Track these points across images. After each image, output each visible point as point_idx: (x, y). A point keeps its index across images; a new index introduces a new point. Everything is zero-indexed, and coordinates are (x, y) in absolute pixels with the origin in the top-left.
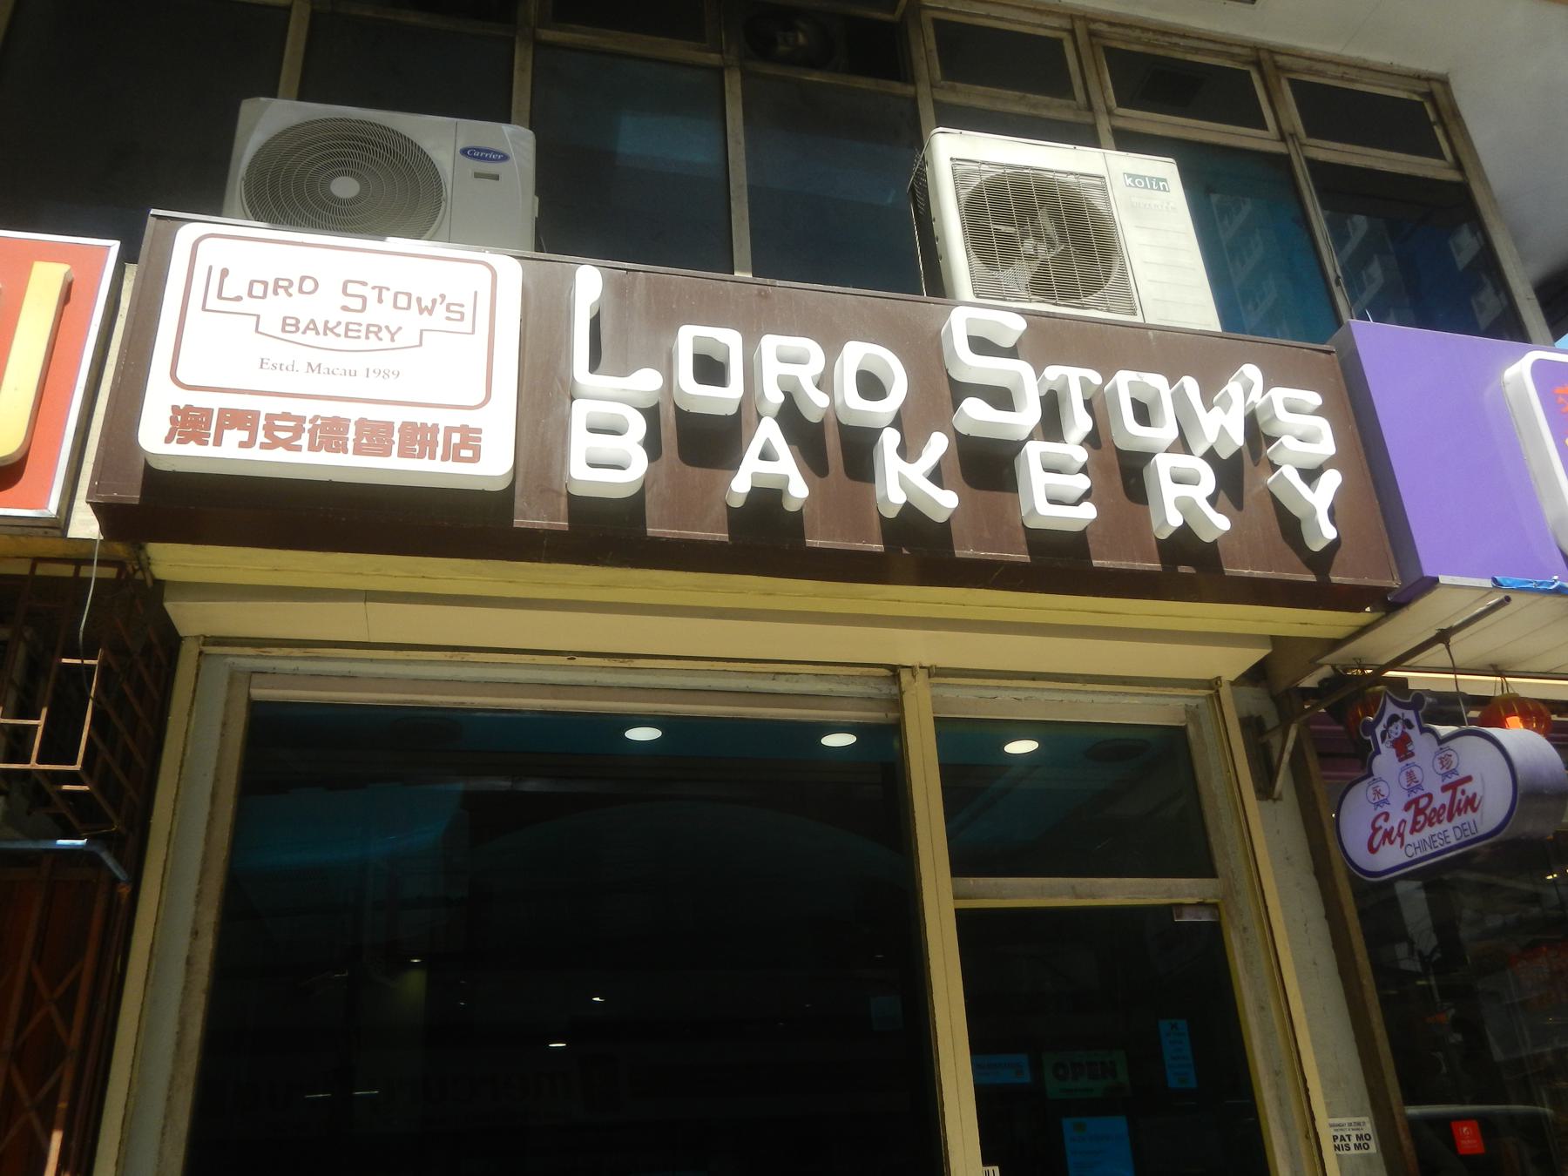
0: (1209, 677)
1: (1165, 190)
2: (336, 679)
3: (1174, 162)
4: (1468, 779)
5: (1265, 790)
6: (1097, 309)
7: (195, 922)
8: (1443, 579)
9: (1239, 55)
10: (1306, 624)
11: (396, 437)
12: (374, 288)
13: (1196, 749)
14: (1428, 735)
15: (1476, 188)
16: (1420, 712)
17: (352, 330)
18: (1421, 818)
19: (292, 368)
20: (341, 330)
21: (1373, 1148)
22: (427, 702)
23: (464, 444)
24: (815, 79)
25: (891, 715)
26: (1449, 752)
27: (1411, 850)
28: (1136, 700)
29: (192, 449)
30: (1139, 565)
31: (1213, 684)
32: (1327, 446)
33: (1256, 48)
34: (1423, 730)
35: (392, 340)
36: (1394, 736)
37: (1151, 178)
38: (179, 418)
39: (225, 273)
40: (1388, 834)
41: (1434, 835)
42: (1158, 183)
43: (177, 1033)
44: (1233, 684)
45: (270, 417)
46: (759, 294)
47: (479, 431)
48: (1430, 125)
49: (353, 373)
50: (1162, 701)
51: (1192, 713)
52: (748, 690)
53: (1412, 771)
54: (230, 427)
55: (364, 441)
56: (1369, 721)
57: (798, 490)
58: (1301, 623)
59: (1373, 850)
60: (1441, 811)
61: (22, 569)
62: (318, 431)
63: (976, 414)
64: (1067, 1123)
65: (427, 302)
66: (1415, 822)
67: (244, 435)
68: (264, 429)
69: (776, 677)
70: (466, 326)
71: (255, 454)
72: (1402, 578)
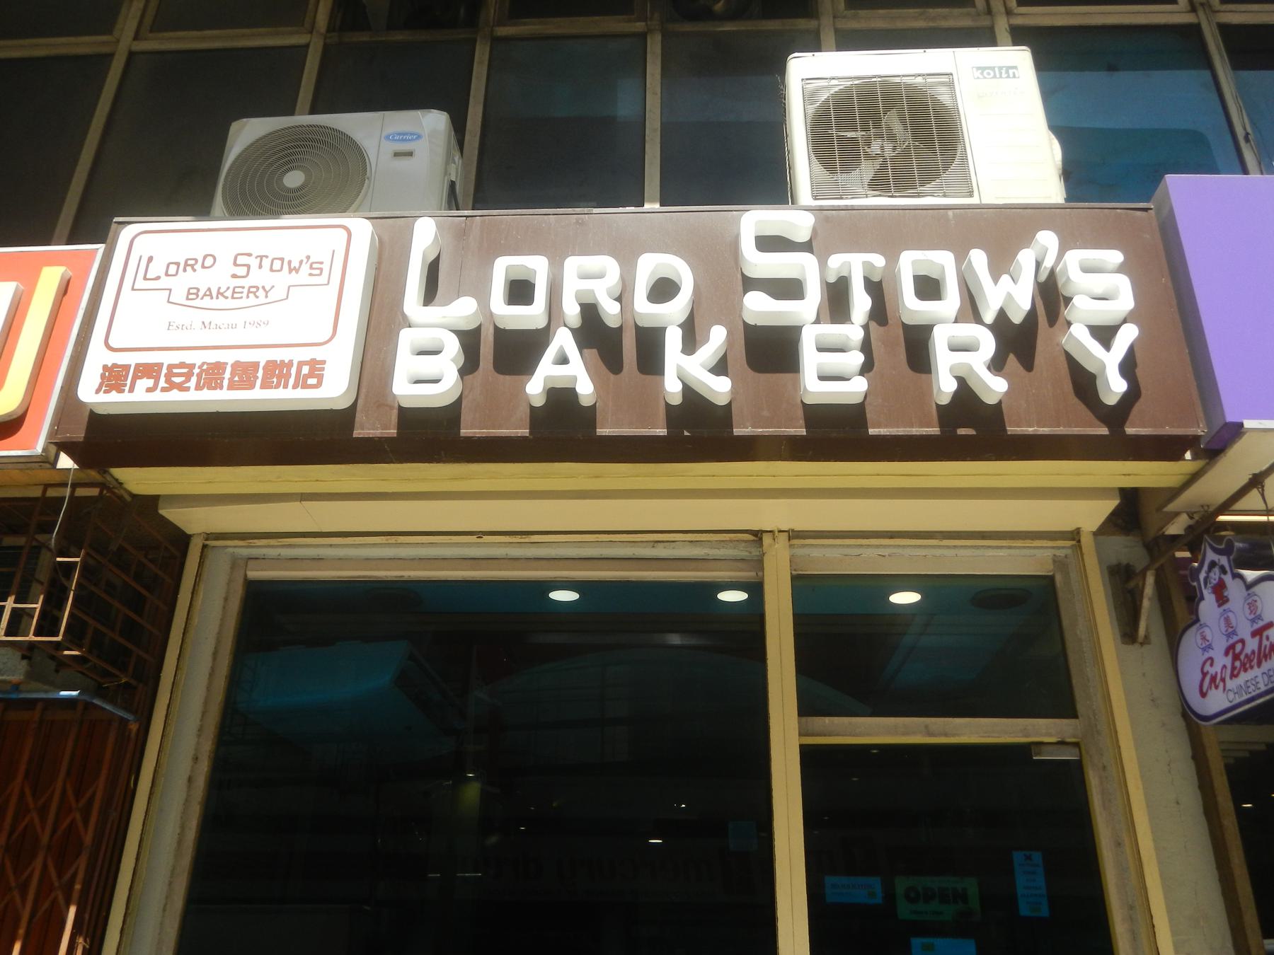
0: (1069, 529)
1: (1014, 77)
2: (308, 561)
3: (1029, 50)
5: (1129, 633)
6: (933, 196)
7: (196, 750)
8: (1248, 424)
10: (1129, 475)
11: (260, 374)
12: (256, 258)
14: (1238, 580)
16: (1231, 557)
17: (237, 293)
18: (1238, 664)
20: (229, 294)
22: (375, 577)
23: (311, 375)
25: (753, 574)
26: (1255, 598)
27: (1231, 696)
28: (1001, 553)
29: (114, 397)
30: (792, 431)
31: (1075, 535)
32: (1125, 301)
35: (266, 297)
37: (1000, 68)
38: (107, 374)
39: (150, 259)
40: (1213, 679)
41: (1248, 681)
42: (1009, 71)
43: (179, 834)
44: (1096, 534)
45: (170, 367)
46: (577, 222)
47: (324, 362)
49: (234, 326)
51: (1059, 563)
52: (603, 557)
53: (1228, 617)
54: (140, 378)
55: (236, 379)
56: (1194, 567)
57: (585, 388)
58: (1124, 475)
59: (1203, 695)
60: (1252, 656)
61: (36, 493)
62: (204, 374)
63: (759, 307)
64: (916, 942)
66: (1233, 668)
67: (150, 383)
68: (165, 376)
69: (656, 544)
70: (323, 279)
71: (158, 396)
72: (1209, 423)
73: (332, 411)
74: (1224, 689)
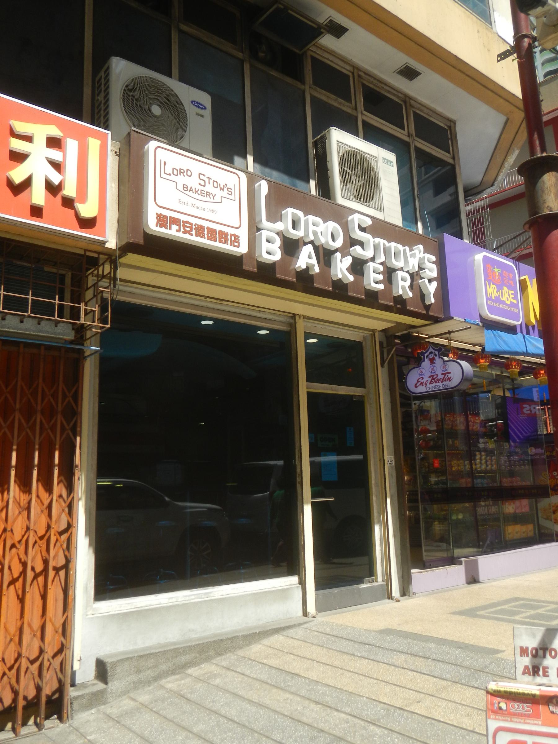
4: (450, 373)
5: (382, 366)
8: (454, 318)
9: (400, 97)
12: (207, 178)
13: (364, 349)
15: (457, 167)
18: (433, 381)
19: (187, 204)
20: (199, 192)
21: (393, 464)
24: (273, 74)
28: (352, 332)
31: (373, 331)
32: (434, 274)
33: (406, 95)
34: (439, 358)
36: (430, 357)
42: (390, 163)
45: (184, 222)
48: (448, 139)
50: (358, 333)
51: (365, 338)
59: (416, 387)
61: (82, 252)
65: (222, 186)
66: (431, 381)
70: (232, 197)
71: (180, 235)
73: (235, 256)
74: (426, 386)
